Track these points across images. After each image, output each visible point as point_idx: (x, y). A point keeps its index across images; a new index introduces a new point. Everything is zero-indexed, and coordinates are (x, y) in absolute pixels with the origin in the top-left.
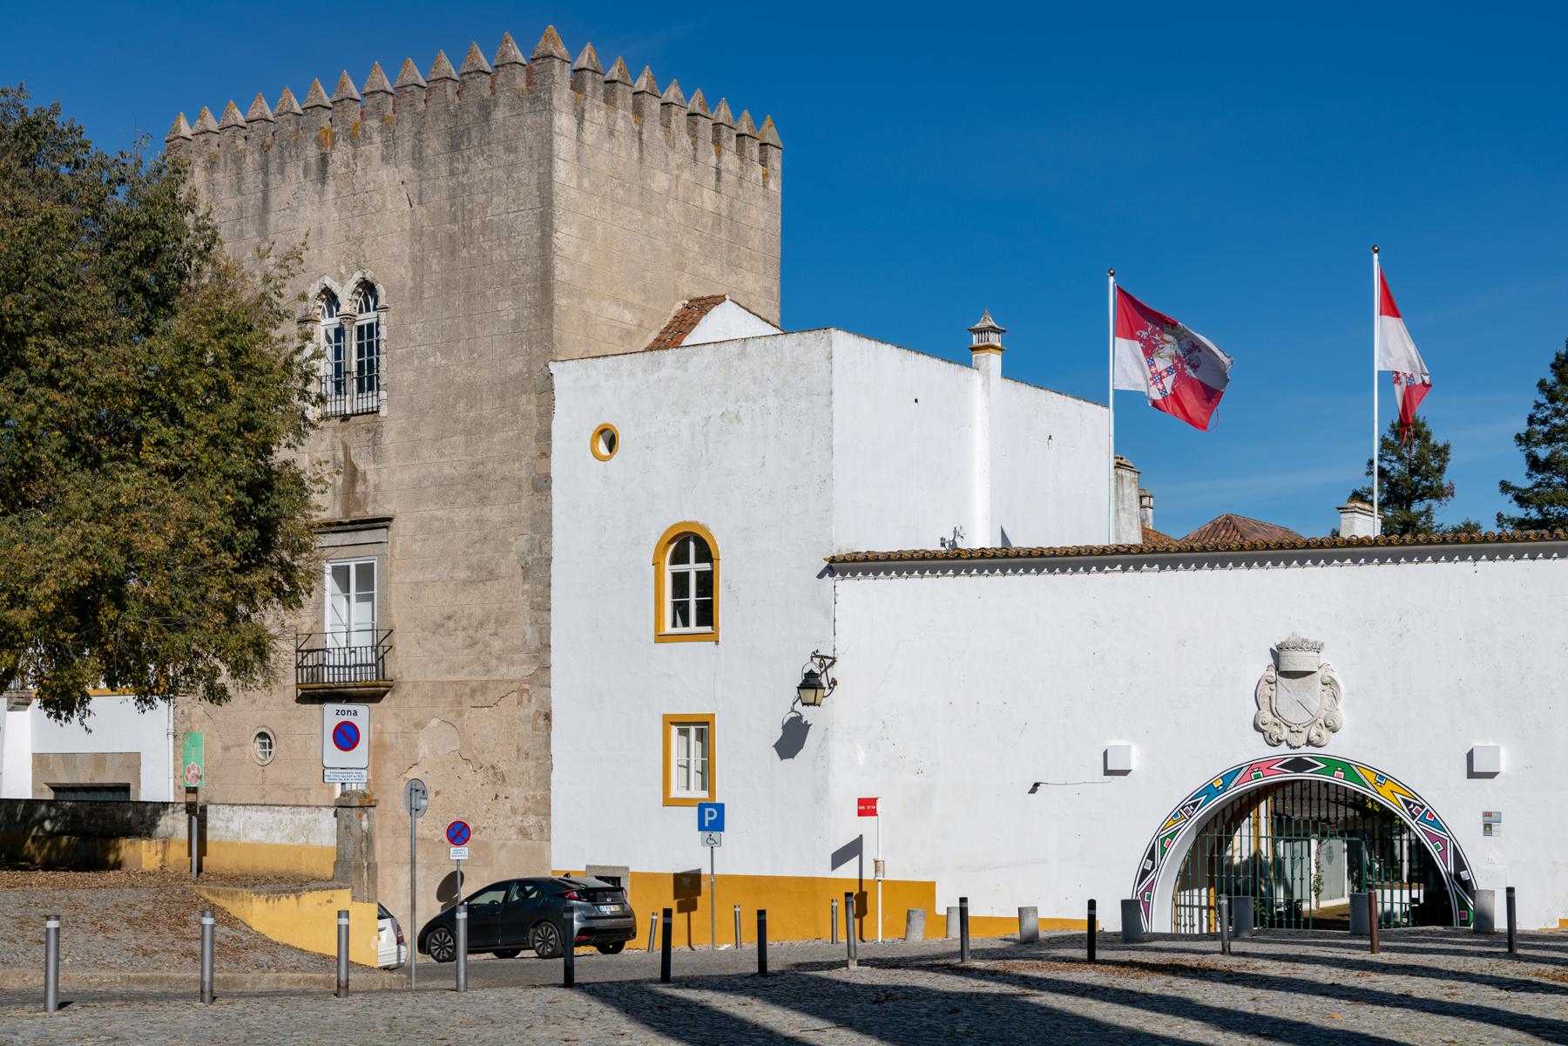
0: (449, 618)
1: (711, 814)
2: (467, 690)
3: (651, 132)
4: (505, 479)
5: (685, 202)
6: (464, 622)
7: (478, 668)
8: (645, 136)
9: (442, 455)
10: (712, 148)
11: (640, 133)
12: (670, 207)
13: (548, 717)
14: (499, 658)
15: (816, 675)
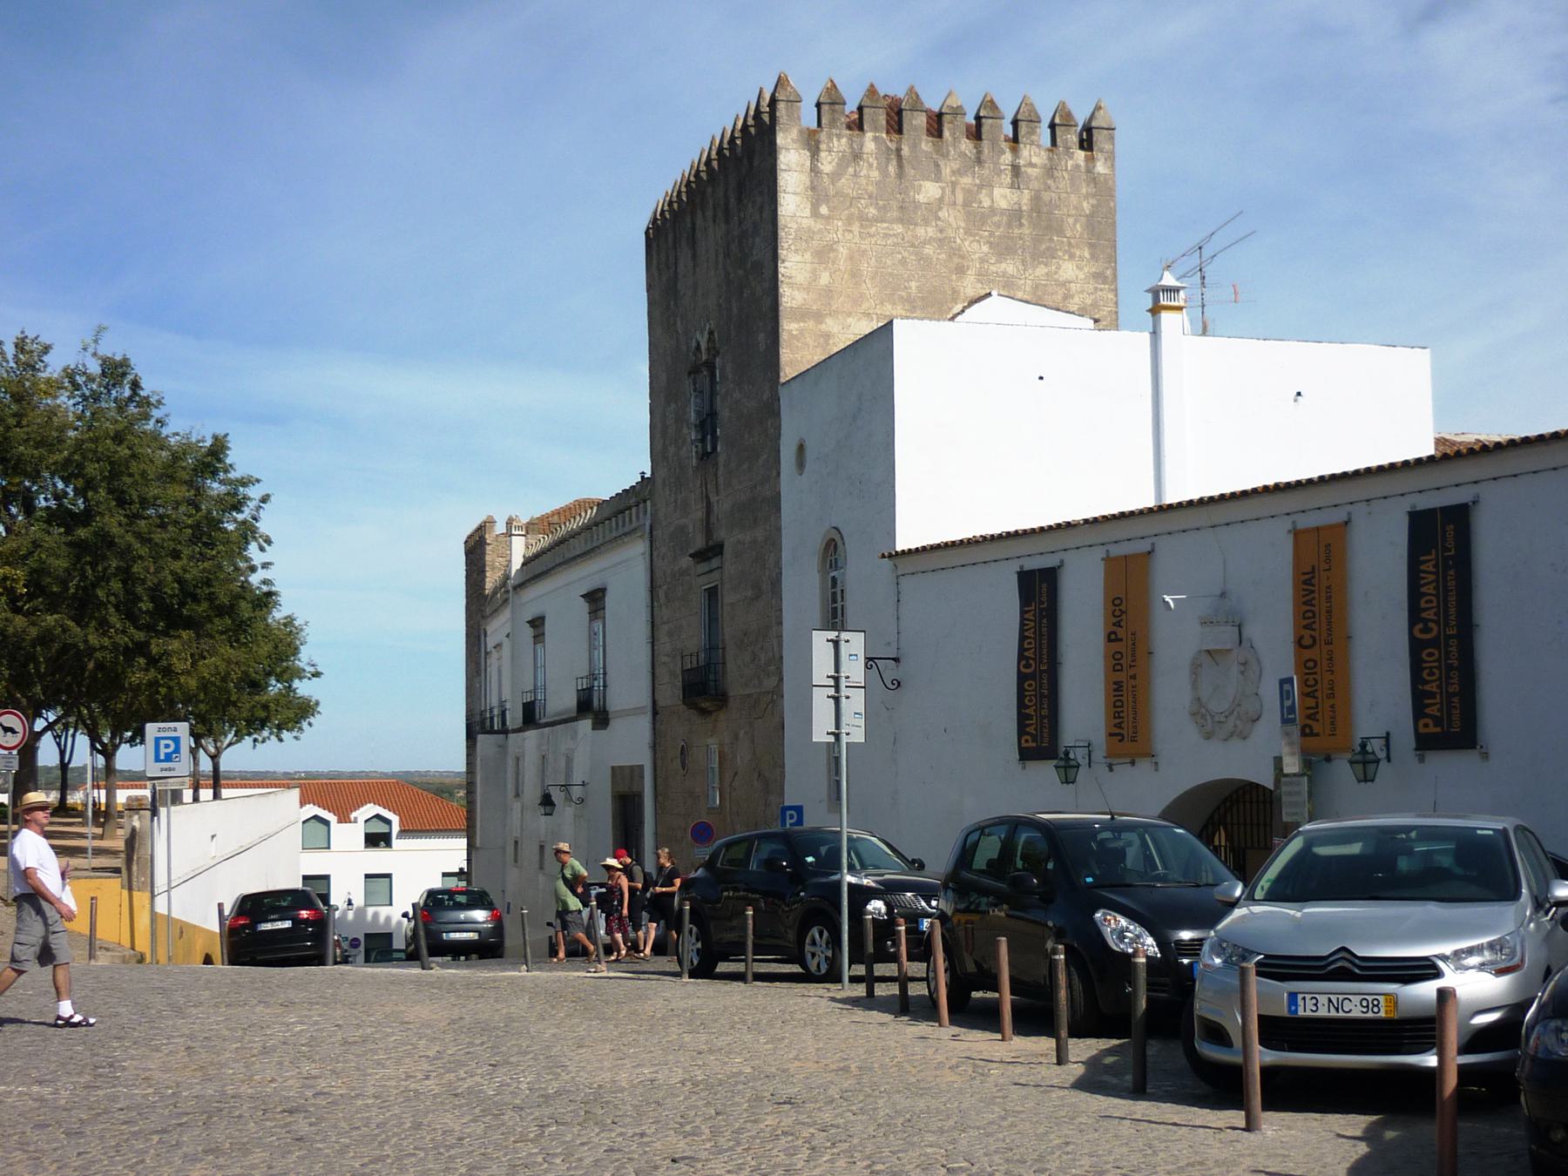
3: (914, 146)
8: (906, 151)
11: (899, 150)
12: (943, 214)
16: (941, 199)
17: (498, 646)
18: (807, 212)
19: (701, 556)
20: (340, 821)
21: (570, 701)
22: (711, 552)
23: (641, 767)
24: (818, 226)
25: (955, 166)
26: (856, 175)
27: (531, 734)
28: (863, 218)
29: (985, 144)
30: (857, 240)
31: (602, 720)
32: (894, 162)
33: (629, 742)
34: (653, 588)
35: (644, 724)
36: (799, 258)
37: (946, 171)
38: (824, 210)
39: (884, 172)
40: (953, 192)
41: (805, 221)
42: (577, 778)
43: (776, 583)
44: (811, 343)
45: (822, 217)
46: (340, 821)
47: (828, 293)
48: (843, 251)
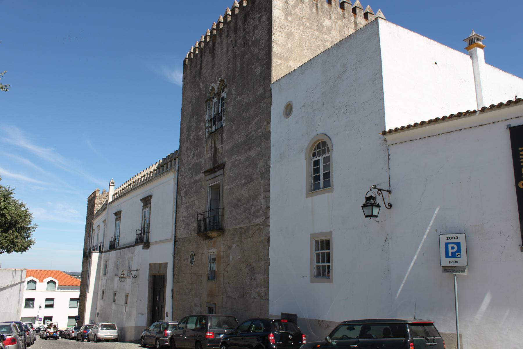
0: (239, 201)
1: (453, 248)
2: (244, 231)
3: (322, 5)
4: (256, 137)
5: (340, 31)
6: (243, 201)
7: (247, 221)
8: (319, 5)
9: (239, 135)
10: (352, 14)
11: (317, 4)
12: (332, 32)
13: (268, 240)
14: (253, 215)
15: (374, 198)
16: (331, 26)
17: (98, 226)
18: (283, 17)
19: (211, 171)
20: (40, 282)
21: (132, 238)
22: (217, 167)
23: (166, 264)
24: (287, 24)
25: (336, 16)
26: (301, 9)
27: (113, 253)
28: (304, 26)
29: (346, 12)
30: (302, 33)
31: (147, 245)
32: (315, 8)
33: (162, 253)
34: (178, 191)
35: (170, 247)
36: (279, 34)
37: (333, 16)
38: (289, 18)
39: (312, 11)
40: (335, 25)
41: (282, 20)
42: (134, 267)
43: (265, 174)
44: (284, 69)
45: (289, 21)
46: (40, 282)
47: (291, 51)
48: (297, 36)
